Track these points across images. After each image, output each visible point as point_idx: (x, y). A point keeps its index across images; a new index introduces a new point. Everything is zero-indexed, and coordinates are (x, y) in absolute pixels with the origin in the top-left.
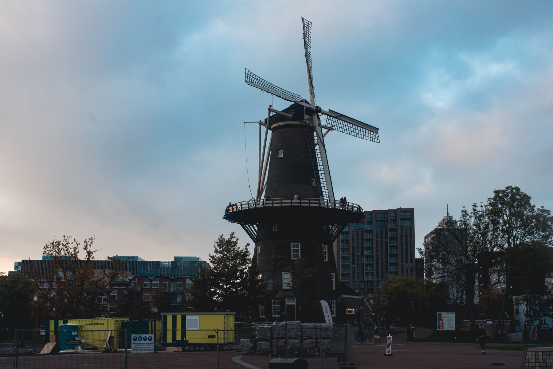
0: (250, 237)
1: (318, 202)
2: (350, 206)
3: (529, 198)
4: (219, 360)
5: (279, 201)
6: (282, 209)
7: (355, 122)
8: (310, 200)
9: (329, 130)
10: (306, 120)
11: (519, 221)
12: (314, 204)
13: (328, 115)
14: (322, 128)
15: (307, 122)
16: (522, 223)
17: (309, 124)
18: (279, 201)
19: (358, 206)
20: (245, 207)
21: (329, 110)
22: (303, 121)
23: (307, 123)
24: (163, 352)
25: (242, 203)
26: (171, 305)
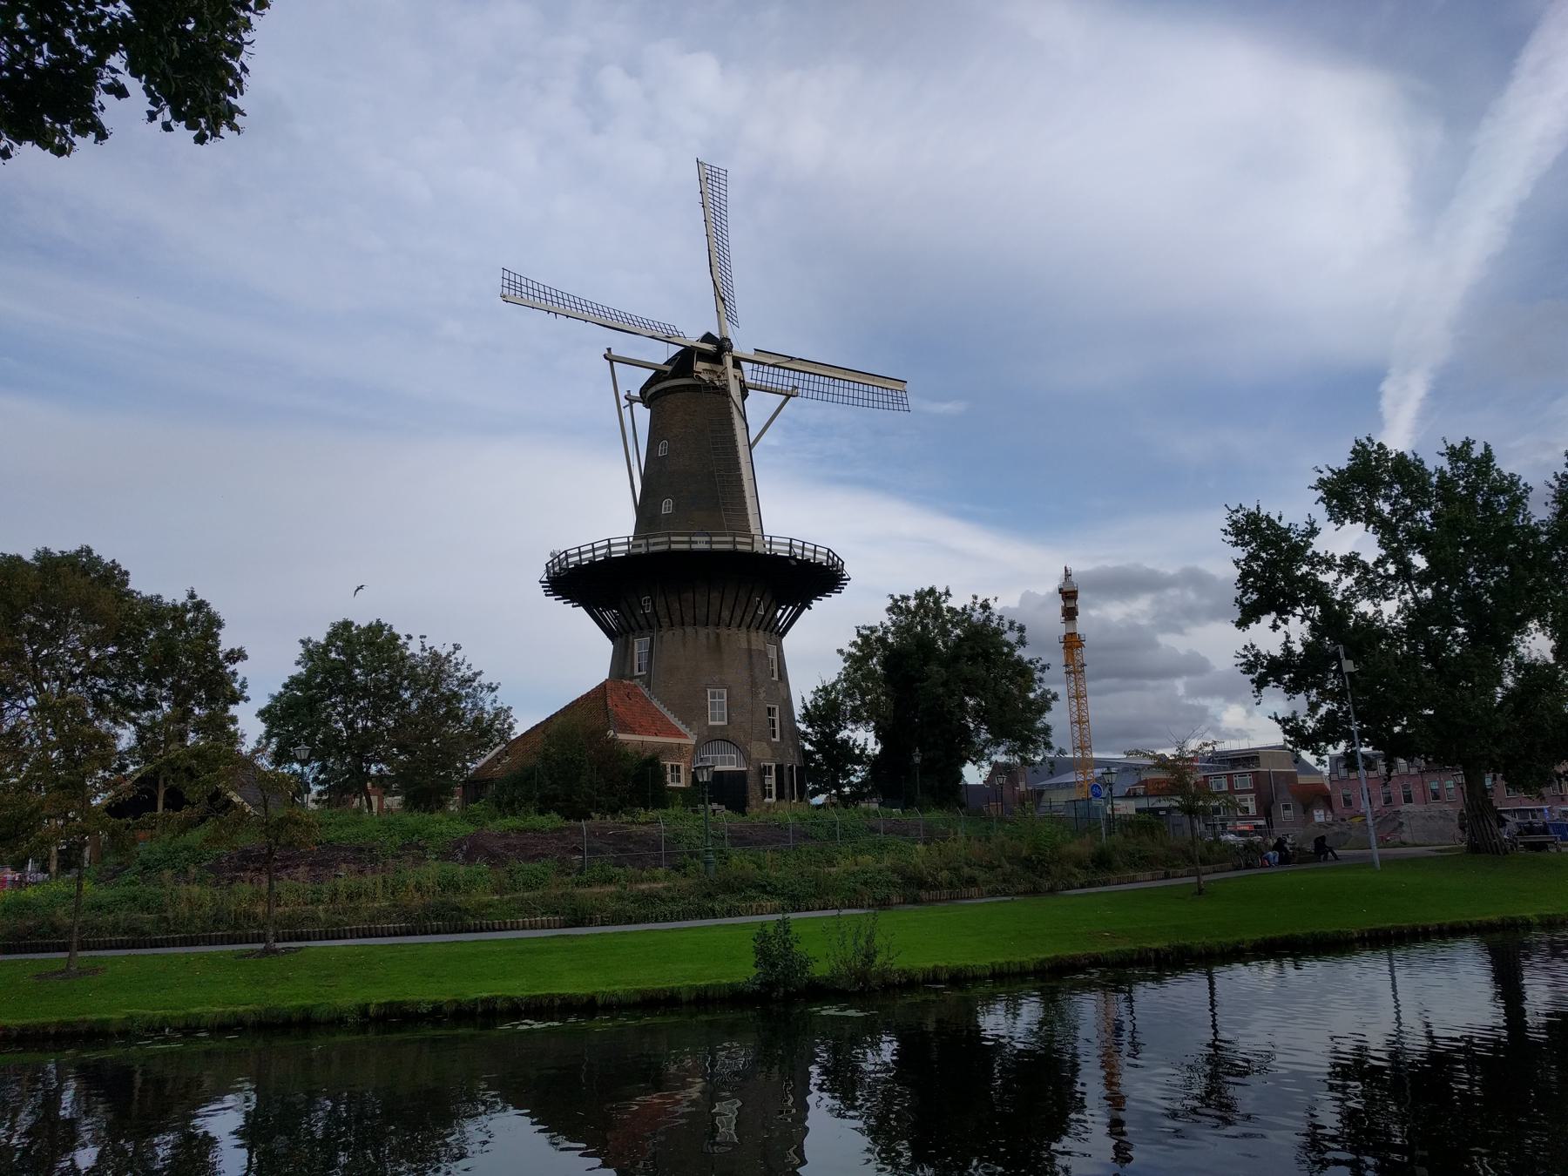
0: (587, 614)
1: (749, 540)
2: (809, 550)
3: (220, 625)
4: (318, 1045)
5: (686, 539)
6: (669, 555)
7: (866, 379)
8: (669, 535)
9: (788, 396)
10: (700, 373)
11: (166, 66)
12: (722, 543)
13: (753, 362)
14: (784, 397)
15: (705, 377)
16: (121, 45)
17: (712, 381)
18: (686, 539)
19: (829, 550)
20: (782, 551)
21: (756, 350)
22: (693, 377)
23: (704, 381)
24: (45, 960)
25: (773, 539)
26: (1457, 620)
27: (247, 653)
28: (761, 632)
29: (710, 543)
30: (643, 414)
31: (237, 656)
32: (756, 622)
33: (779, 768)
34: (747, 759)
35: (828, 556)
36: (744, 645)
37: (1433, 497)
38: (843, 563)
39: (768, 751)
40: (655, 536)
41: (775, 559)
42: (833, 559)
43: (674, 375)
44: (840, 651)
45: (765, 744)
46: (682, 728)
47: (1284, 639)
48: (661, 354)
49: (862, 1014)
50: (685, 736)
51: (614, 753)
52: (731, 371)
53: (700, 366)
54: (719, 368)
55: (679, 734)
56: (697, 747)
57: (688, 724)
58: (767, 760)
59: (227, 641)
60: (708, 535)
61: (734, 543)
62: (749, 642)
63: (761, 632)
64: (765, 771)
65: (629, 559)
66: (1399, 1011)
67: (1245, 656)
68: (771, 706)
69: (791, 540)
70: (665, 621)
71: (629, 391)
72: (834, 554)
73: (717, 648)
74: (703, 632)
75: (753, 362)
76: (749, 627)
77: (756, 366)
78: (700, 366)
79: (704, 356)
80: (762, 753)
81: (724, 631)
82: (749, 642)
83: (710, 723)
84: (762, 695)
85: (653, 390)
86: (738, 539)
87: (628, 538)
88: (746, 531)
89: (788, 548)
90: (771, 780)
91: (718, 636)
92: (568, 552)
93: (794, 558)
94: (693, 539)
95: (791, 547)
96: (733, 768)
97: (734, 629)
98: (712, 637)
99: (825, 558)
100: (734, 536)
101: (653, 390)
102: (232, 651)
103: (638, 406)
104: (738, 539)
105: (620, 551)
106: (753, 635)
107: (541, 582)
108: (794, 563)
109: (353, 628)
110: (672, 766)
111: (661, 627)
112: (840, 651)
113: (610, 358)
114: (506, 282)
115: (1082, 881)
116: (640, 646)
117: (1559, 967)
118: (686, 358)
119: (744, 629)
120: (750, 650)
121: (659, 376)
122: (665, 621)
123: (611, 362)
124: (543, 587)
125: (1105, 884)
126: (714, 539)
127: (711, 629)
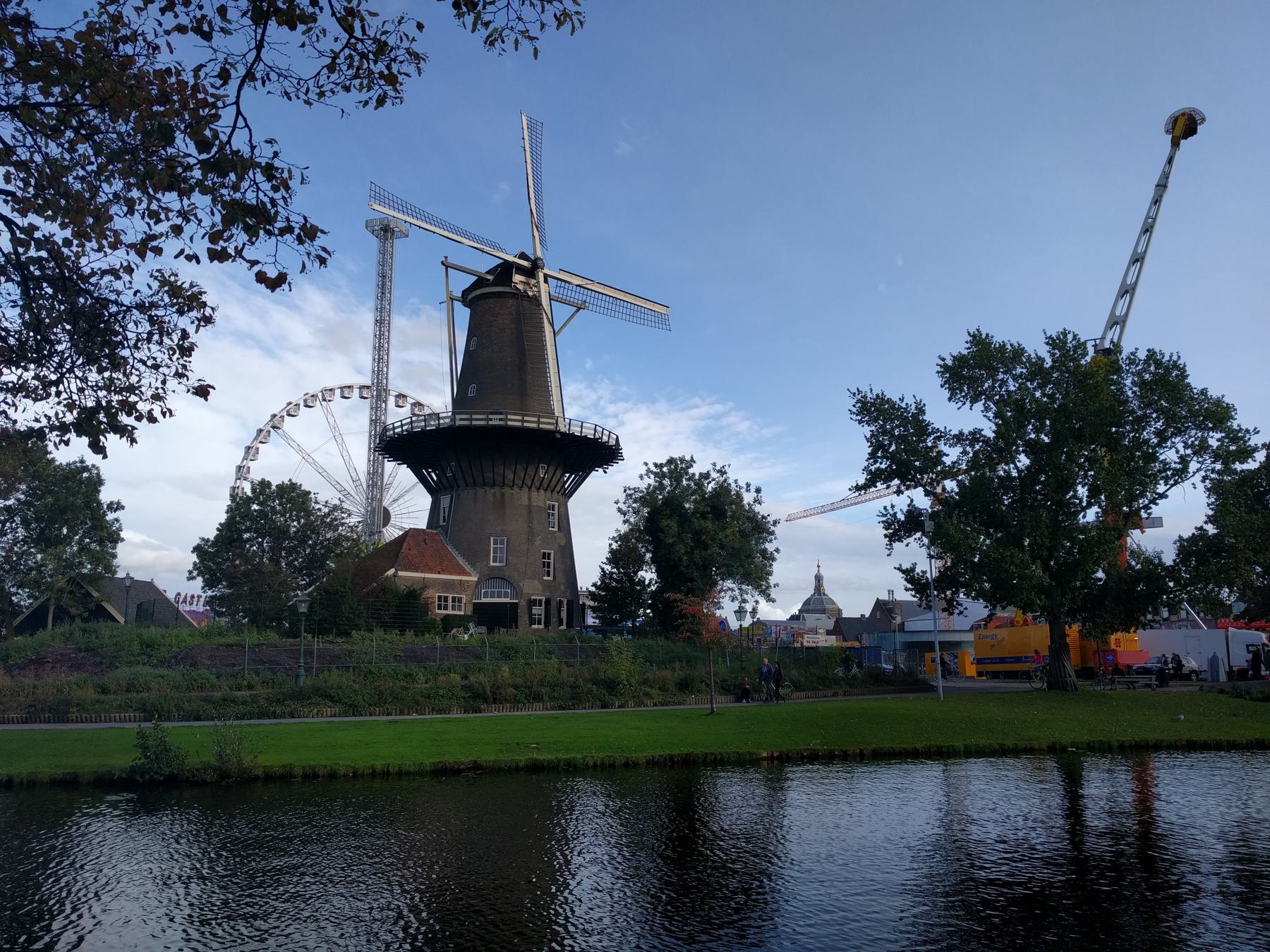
0: (588, 479)
1: (554, 421)
5: (520, 418)
9: (579, 309)
15: (520, 287)
17: (525, 291)
18: (520, 418)
27: (123, 504)
28: (542, 492)
29: (523, 421)
30: (463, 314)
31: (116, 506)
32: (537, 483)
33: (548, 602)
34: (517, 592)
36: (525, 502)
37: (84, 169)
39: (540, 587)
41: (569, 438)
43: (495, 284)
45: (536, 582)
46: (467, 568)
47: (908, 501)
48: (484, 265)
50: (469, 574)
51: (386, 588)
52: (543, 286)
53: (517, 278)
54: (533, 282)
55: (464, 573)
56: (478, 583)
57: (472, 564)
58: (538, 595)
59: (106, 496)
60: (467, 413)
61: (506, 420)
62: (530, 500)
63: (542, 492)
64: (532, 603)
65: (441, 432)
67: (886, 515)
68: (547, 551)
70: (461, 482)
71: (446, 257)
73: (501, 504)
74: (490, 492)
76: (530, 488)
78: (517, 278)
79: (521, 270)
80: (533, 589)
81: (508, 491)
82: (530, 500)
83: (492, 564)
84: (538, 542)
85: (473, 294)
86: (541, 420)
88: (551, 413)
90: (538, 611)
91: (503, 494)
93: (559, 432)
94: (490, 417)
96: (507, 600)
97: (516, 490)
98: (498, 495)
100: (539, 417)
101: (473, 294)
102: (112, 503)
103: (458, 305)
104: (541, 420)
105: (445, 422)
106: (534, 494)
108: (558, 436)
110: (454, 599)
111: (459, 487)
113: (446, 265)
114: (373, 193)
115: (656, 701)
116: (445, 501)
117: (667, 946)
118: (504, 270)
119: (525, 489)
120: (529, 508)
121: (480, 282)
122: (461, 482)
123: (447, 267)
125: (680, 704)
126: (474, 417)
127: (497, 489)
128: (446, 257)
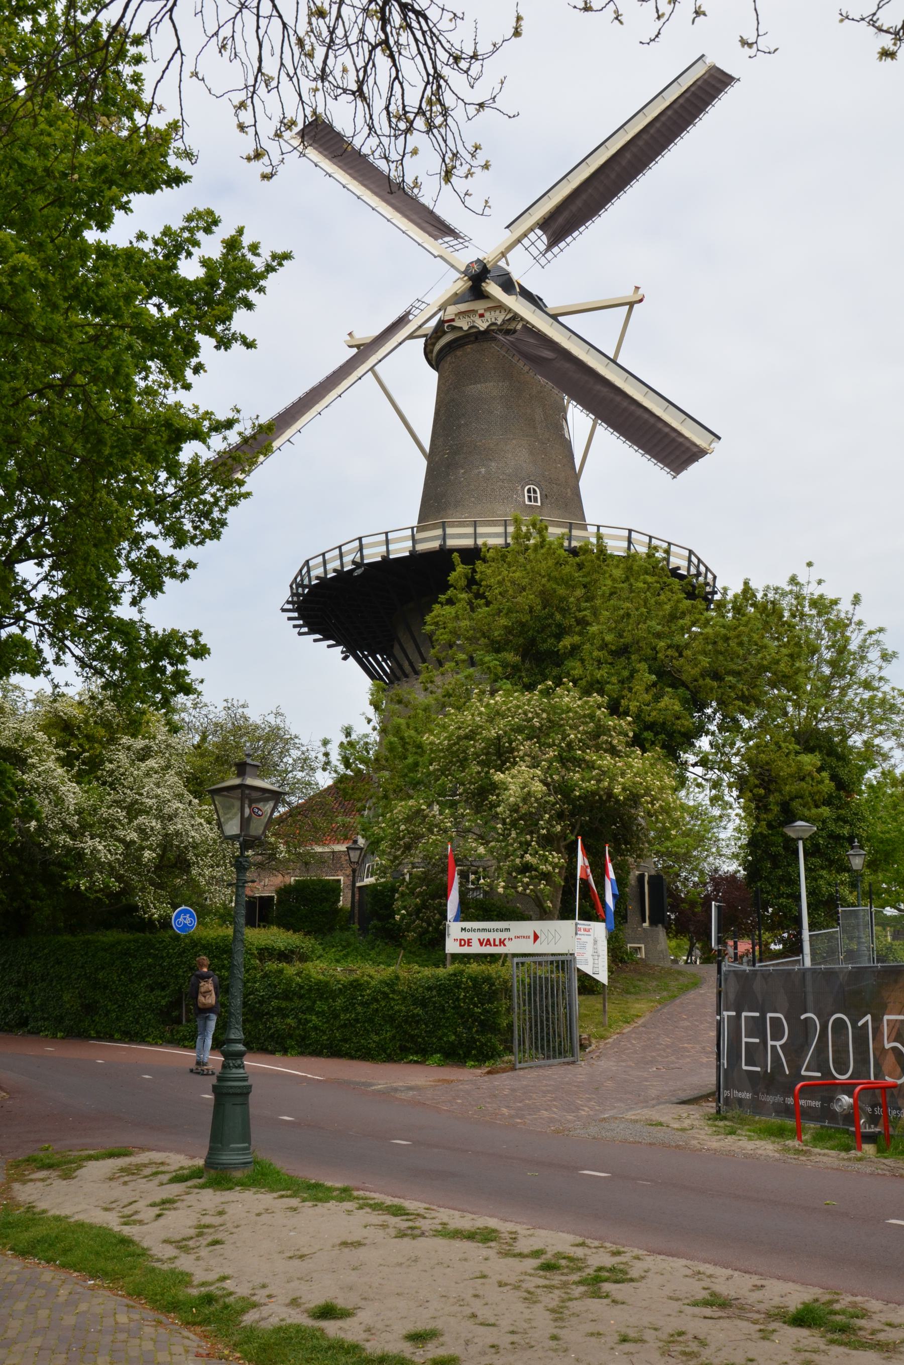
9: (631, 305)
10: (453, 320)
13: (519, 241)
21: (508, 227)
23: (461, 328)
35: (690, 561)
38: (715, 577)
40: (453, 525)
42: (698, 567)
44: (240, 231)
49: (610, 866)
66: (273, 269)
69: (630, 531)
71: (350, 334)
72: (707, 569)
75: (519, 241)
77: (526, 242)
87: (412, 528)
89: (625, 544)
92: (311, 563)
95: (630, 542)
99: (685, 564)
105: (401, 549)
107: (284, 610)
109: (54, 596)
112: (240, 231)
124: (290, 619)
128: (350, 334)
